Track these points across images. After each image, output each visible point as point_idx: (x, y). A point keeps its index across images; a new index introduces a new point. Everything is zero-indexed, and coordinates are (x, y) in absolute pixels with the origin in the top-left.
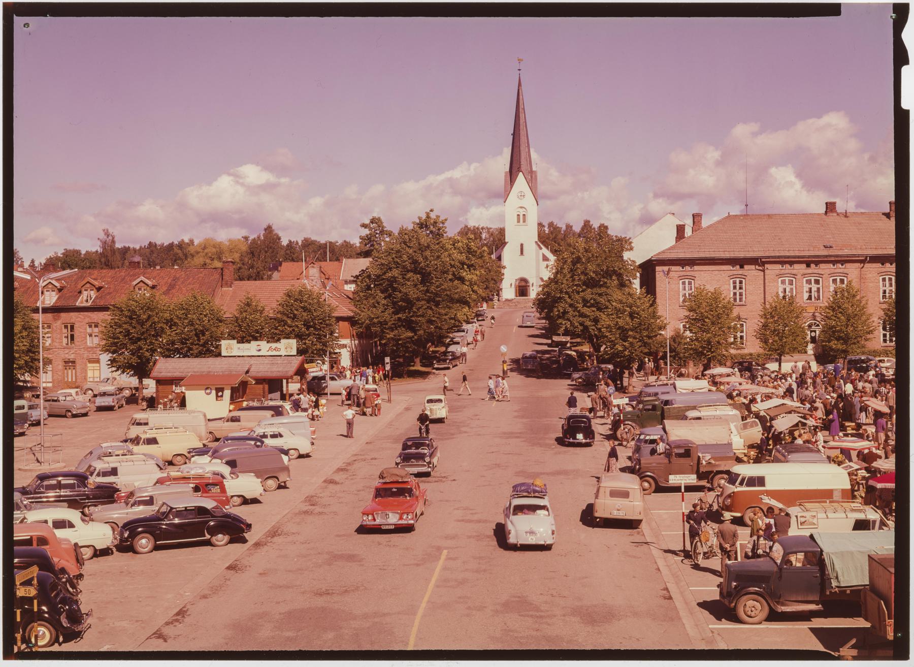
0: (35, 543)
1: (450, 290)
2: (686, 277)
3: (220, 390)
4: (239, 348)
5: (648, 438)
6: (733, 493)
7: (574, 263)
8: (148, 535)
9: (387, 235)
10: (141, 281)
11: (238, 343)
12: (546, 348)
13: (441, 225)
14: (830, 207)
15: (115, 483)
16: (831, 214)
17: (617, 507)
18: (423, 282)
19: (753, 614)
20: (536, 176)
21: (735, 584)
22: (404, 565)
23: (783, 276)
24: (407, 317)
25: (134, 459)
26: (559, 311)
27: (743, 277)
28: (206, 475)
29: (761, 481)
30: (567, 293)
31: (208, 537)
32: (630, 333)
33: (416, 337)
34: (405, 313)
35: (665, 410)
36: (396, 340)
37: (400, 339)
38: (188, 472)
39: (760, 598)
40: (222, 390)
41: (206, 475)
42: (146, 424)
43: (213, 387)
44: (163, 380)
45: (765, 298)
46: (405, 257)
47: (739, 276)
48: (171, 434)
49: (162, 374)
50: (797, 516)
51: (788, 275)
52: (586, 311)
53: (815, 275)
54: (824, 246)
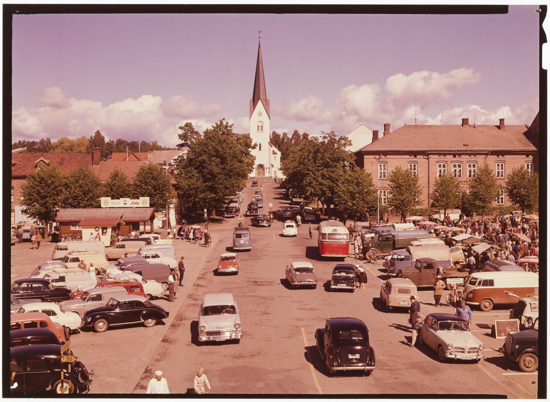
0: (39, 325)
1: (238, 168)
2: (382, 162)
3: (104, 228)
4: (112, 203)
5: (399, 257)
6: (474, 290)
7: (315, 153)
8: (104, 320)
9: (195, 134)
10: (42, 160)
11: (112, 199)
12: (288, 205)
13: (229, 128)
14: (465, 122)
15: (65, 286)
16: (466, 126)
17: (403, 299)
18: (222, 163)
19: (530, 366)
20: (269, 103)
21: (518, 346)
22: (281, 338)
23: (440, 162)
24: (211, 184)
25: (76, 271)
26: (307, 182)
27: (416, 162)
28: (131, 281)
29: (491, 282)
30: (311, 171)
31: (143, 321)
32: (357, 195)
33: (217, 197)
34: (210, 182)
35: (396, 241)
36: (205, 199)
37: (207, 199)
38: (119, 279)
39: (534, 356)
40: (106, 228)
41: (131, 281)
42: (66, 249)
43: (100, 227)
44: (64, 223)
45: (429, 175)
46: (210, 148)
47: (414, 162)
48: (88, 255)
49: (64, 218)
50: (530, 304)
51: (443, 162)
52: (324, 182)
53: (459, 162)
54: (464, 145)
